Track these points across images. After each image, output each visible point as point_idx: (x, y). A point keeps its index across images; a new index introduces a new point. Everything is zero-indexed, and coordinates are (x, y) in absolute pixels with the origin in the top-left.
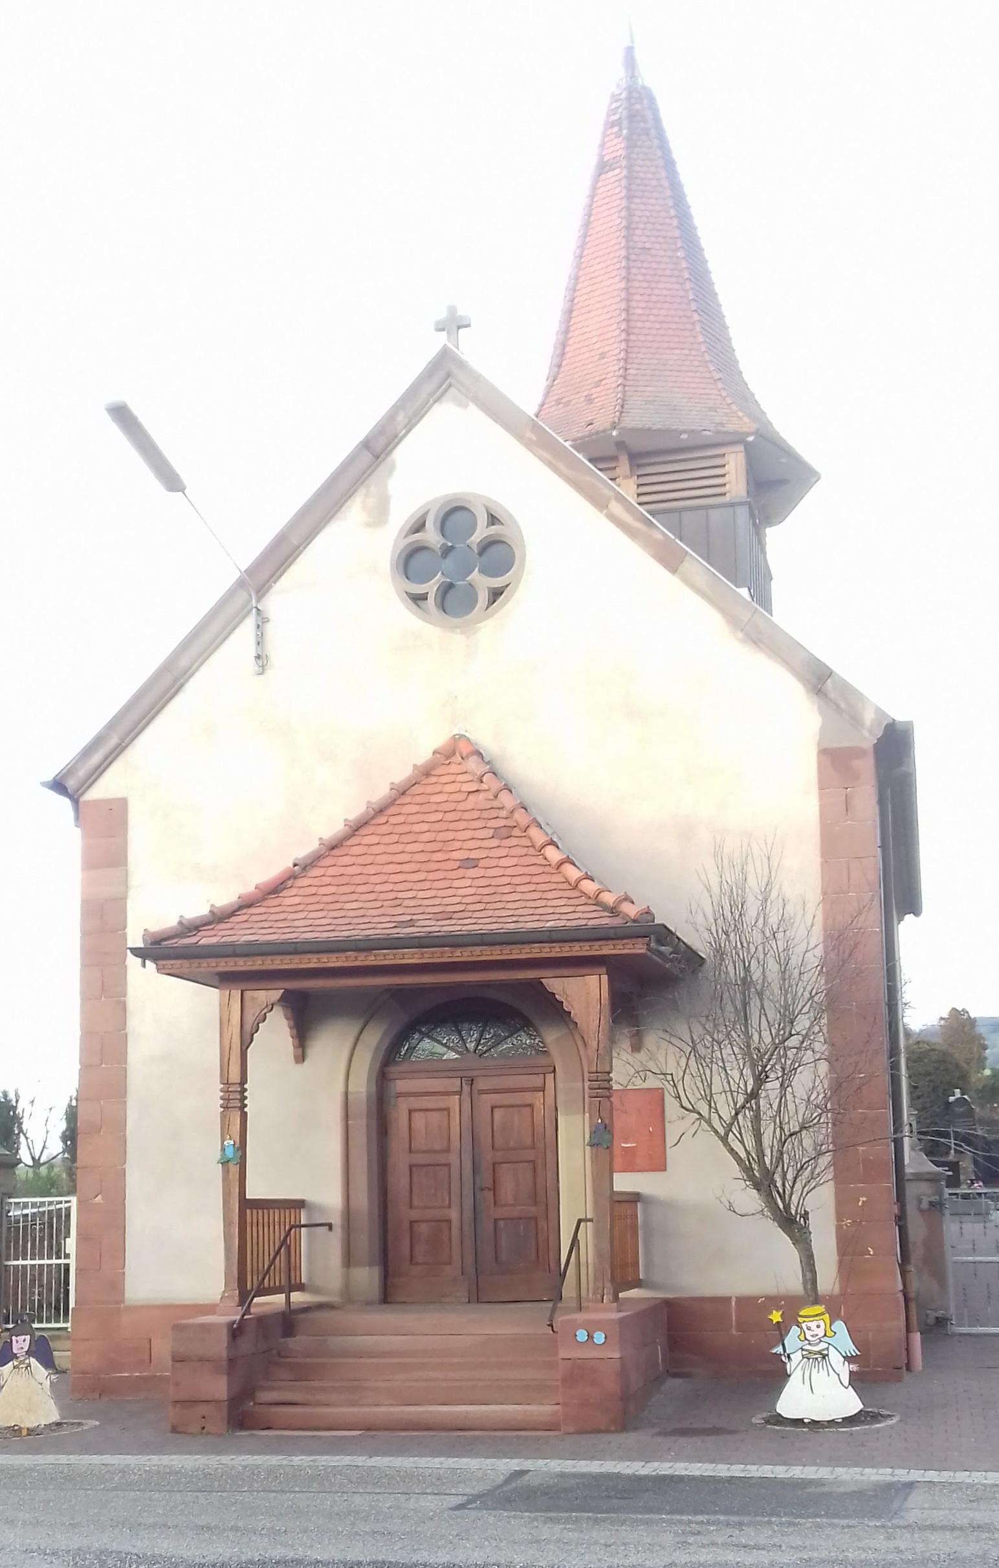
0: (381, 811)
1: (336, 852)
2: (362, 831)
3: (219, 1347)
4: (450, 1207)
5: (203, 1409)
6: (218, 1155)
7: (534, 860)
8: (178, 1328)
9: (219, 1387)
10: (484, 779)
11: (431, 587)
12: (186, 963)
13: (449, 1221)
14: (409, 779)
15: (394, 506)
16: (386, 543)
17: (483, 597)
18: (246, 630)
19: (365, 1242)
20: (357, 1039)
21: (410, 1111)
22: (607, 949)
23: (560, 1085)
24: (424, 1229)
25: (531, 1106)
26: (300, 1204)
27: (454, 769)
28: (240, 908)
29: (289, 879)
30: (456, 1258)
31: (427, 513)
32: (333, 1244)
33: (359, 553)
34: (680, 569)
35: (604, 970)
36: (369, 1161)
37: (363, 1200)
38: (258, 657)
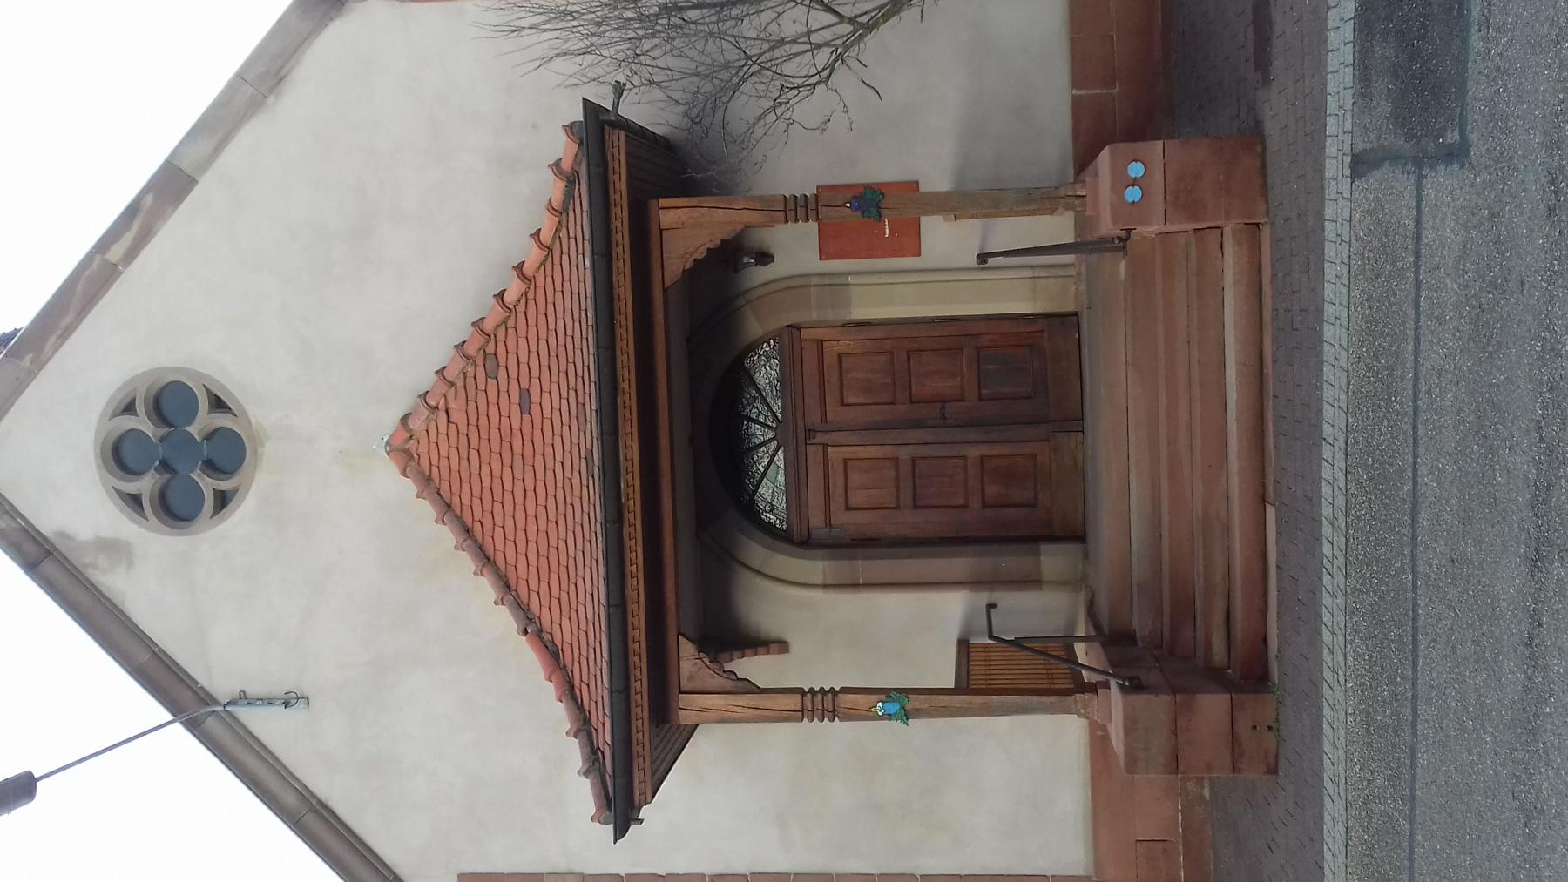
0: (468, 532)
1: (513, 583)
2: (490, 552)
3: (1157, 705)
4: (964, 458)
5: (1243, 729)
6: (897, 725)
7: (521, 316)
8: (1132, 763)
9: (1212, 706)
10: (433, 404)
11: (208, 485)
12: (638, 762)
13: (982, 458)
14: (432, 502)
15: (107, 533)
16: (153, 543)
17: (222, 420)
18: (254, 719)
19: (1011, 561)
20: (759, 573)
21: (848, 508)
22: (620, 184)
23: (814, 316)
24: (992, 490)
25: (840, 357)
26: (964, 645)
27: (423, 449)
28: (573, 697)
29: (541, 638)
30: (1027, 449)
31: (118, 492)
32: (1010, 600)
33: (158, 574)
34: (189, 171)
35: (653, 203)
36: (910, 557)
37: (959, 564)
38: (287, 704)
